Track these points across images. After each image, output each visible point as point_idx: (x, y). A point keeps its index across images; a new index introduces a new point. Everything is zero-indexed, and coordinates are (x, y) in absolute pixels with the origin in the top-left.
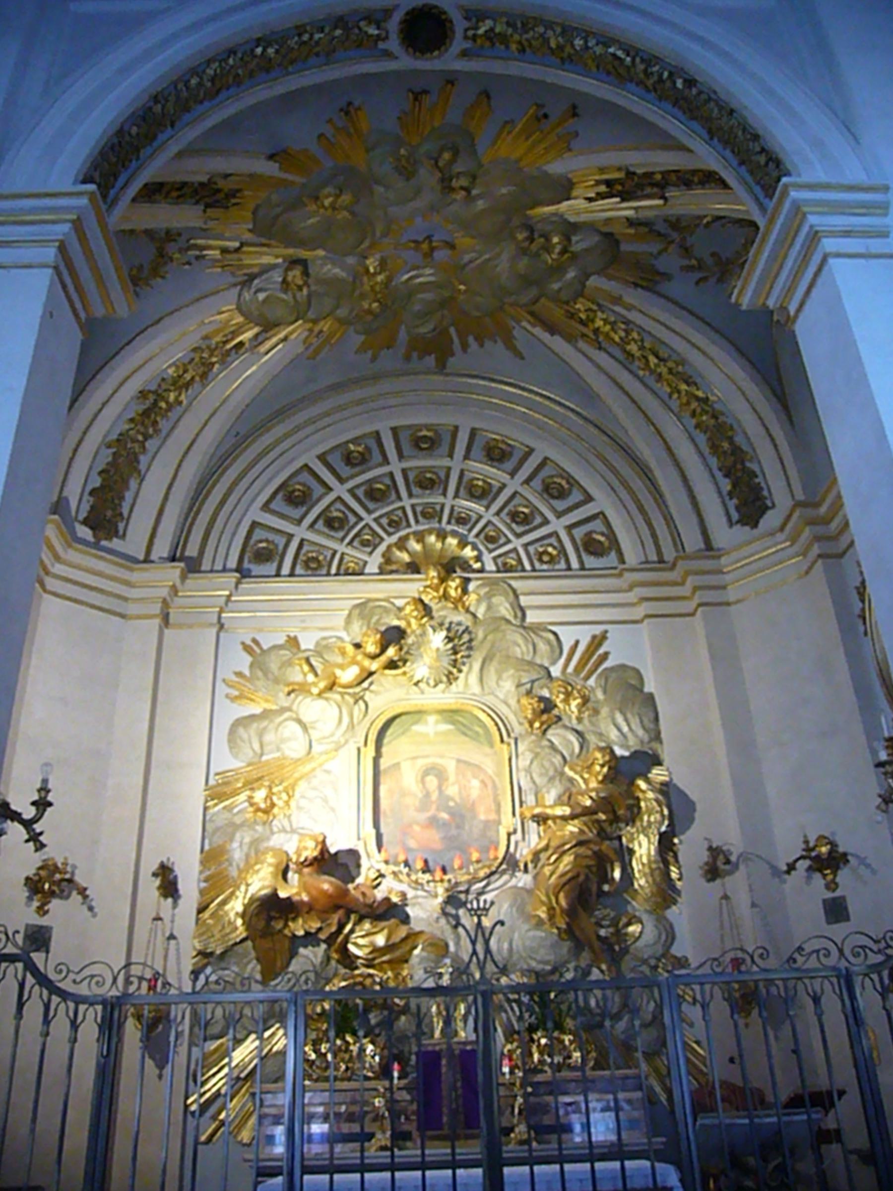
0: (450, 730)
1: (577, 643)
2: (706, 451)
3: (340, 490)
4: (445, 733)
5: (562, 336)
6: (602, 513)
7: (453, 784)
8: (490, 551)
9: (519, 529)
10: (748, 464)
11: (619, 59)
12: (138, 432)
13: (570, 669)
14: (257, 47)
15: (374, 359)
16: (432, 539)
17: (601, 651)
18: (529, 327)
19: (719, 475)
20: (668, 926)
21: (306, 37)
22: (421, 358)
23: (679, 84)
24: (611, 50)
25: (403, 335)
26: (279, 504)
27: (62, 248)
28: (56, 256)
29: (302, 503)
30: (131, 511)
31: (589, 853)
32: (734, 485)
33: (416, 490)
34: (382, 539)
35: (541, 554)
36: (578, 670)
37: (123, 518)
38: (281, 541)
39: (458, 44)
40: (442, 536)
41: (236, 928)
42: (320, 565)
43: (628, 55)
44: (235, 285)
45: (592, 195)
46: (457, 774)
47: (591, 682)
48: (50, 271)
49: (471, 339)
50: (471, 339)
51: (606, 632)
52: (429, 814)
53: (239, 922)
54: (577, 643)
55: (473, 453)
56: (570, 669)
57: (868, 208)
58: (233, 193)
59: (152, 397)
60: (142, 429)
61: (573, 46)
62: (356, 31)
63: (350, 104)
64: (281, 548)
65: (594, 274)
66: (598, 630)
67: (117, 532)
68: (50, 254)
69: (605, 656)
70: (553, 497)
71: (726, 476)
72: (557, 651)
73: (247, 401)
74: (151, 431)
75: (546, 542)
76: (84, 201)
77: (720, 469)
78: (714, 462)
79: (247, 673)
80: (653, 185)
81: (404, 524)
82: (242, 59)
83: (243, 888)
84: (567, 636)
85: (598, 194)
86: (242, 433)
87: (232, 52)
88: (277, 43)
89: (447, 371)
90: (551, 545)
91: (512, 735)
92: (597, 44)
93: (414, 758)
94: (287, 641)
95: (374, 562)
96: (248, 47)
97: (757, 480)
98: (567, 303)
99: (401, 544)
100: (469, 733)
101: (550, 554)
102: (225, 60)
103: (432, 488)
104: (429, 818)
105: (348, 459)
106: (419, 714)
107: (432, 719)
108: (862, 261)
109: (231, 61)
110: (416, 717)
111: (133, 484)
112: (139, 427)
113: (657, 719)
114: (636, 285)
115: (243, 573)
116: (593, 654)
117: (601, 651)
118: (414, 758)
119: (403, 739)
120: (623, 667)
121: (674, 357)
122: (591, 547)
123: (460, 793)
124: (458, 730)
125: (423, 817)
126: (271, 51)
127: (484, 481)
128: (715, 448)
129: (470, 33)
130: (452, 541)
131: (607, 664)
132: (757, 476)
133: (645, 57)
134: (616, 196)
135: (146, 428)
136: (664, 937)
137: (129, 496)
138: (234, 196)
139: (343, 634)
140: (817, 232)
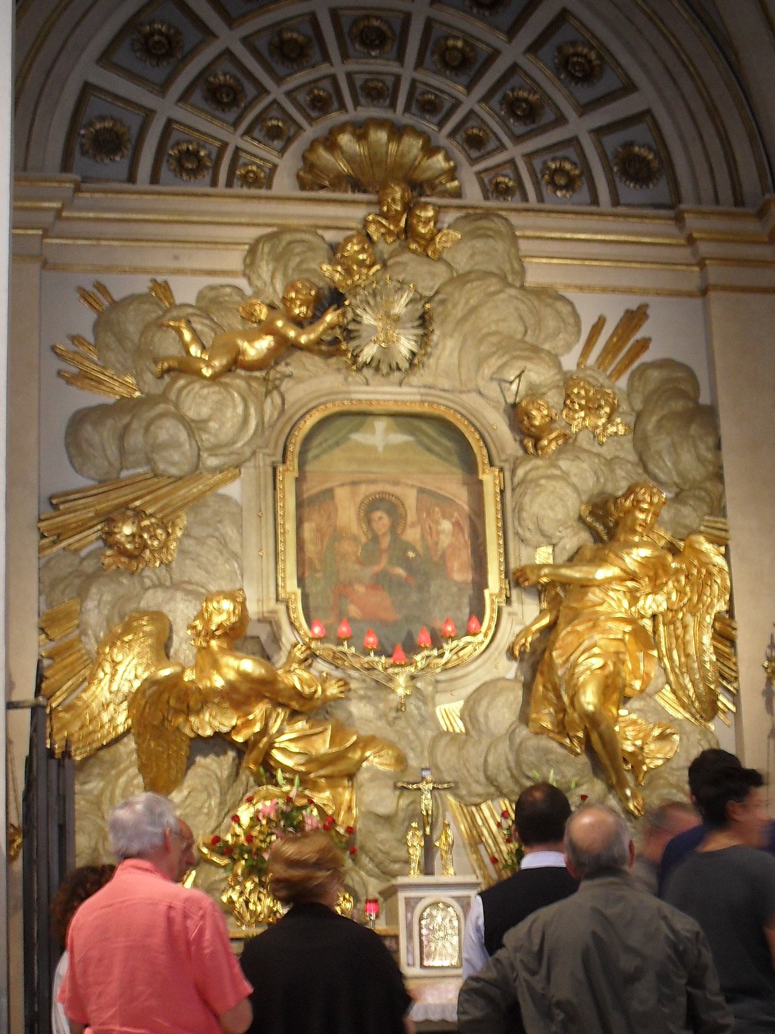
0: (406, 443)
4: (400, 448)
7: (413, 525)
9: (519, 129)
36: (602, 361)
38: (133, 121)
46: (419, 511)
52: (376, 568)
64: (134, 131)
69: (644, 345)
75: (560, 154)
83: (108, 668)
90: (566, 159)
93: (354, 483)
104: (377, 575)
107: (380, 425)
110: (357, 420)
113: (718, 446)
117: (638, 335)
118: (354, 483)
119: (337, 453)
123: (423, 537)
124: (420, 443)
131: (646, 357)
139: (242, 283)
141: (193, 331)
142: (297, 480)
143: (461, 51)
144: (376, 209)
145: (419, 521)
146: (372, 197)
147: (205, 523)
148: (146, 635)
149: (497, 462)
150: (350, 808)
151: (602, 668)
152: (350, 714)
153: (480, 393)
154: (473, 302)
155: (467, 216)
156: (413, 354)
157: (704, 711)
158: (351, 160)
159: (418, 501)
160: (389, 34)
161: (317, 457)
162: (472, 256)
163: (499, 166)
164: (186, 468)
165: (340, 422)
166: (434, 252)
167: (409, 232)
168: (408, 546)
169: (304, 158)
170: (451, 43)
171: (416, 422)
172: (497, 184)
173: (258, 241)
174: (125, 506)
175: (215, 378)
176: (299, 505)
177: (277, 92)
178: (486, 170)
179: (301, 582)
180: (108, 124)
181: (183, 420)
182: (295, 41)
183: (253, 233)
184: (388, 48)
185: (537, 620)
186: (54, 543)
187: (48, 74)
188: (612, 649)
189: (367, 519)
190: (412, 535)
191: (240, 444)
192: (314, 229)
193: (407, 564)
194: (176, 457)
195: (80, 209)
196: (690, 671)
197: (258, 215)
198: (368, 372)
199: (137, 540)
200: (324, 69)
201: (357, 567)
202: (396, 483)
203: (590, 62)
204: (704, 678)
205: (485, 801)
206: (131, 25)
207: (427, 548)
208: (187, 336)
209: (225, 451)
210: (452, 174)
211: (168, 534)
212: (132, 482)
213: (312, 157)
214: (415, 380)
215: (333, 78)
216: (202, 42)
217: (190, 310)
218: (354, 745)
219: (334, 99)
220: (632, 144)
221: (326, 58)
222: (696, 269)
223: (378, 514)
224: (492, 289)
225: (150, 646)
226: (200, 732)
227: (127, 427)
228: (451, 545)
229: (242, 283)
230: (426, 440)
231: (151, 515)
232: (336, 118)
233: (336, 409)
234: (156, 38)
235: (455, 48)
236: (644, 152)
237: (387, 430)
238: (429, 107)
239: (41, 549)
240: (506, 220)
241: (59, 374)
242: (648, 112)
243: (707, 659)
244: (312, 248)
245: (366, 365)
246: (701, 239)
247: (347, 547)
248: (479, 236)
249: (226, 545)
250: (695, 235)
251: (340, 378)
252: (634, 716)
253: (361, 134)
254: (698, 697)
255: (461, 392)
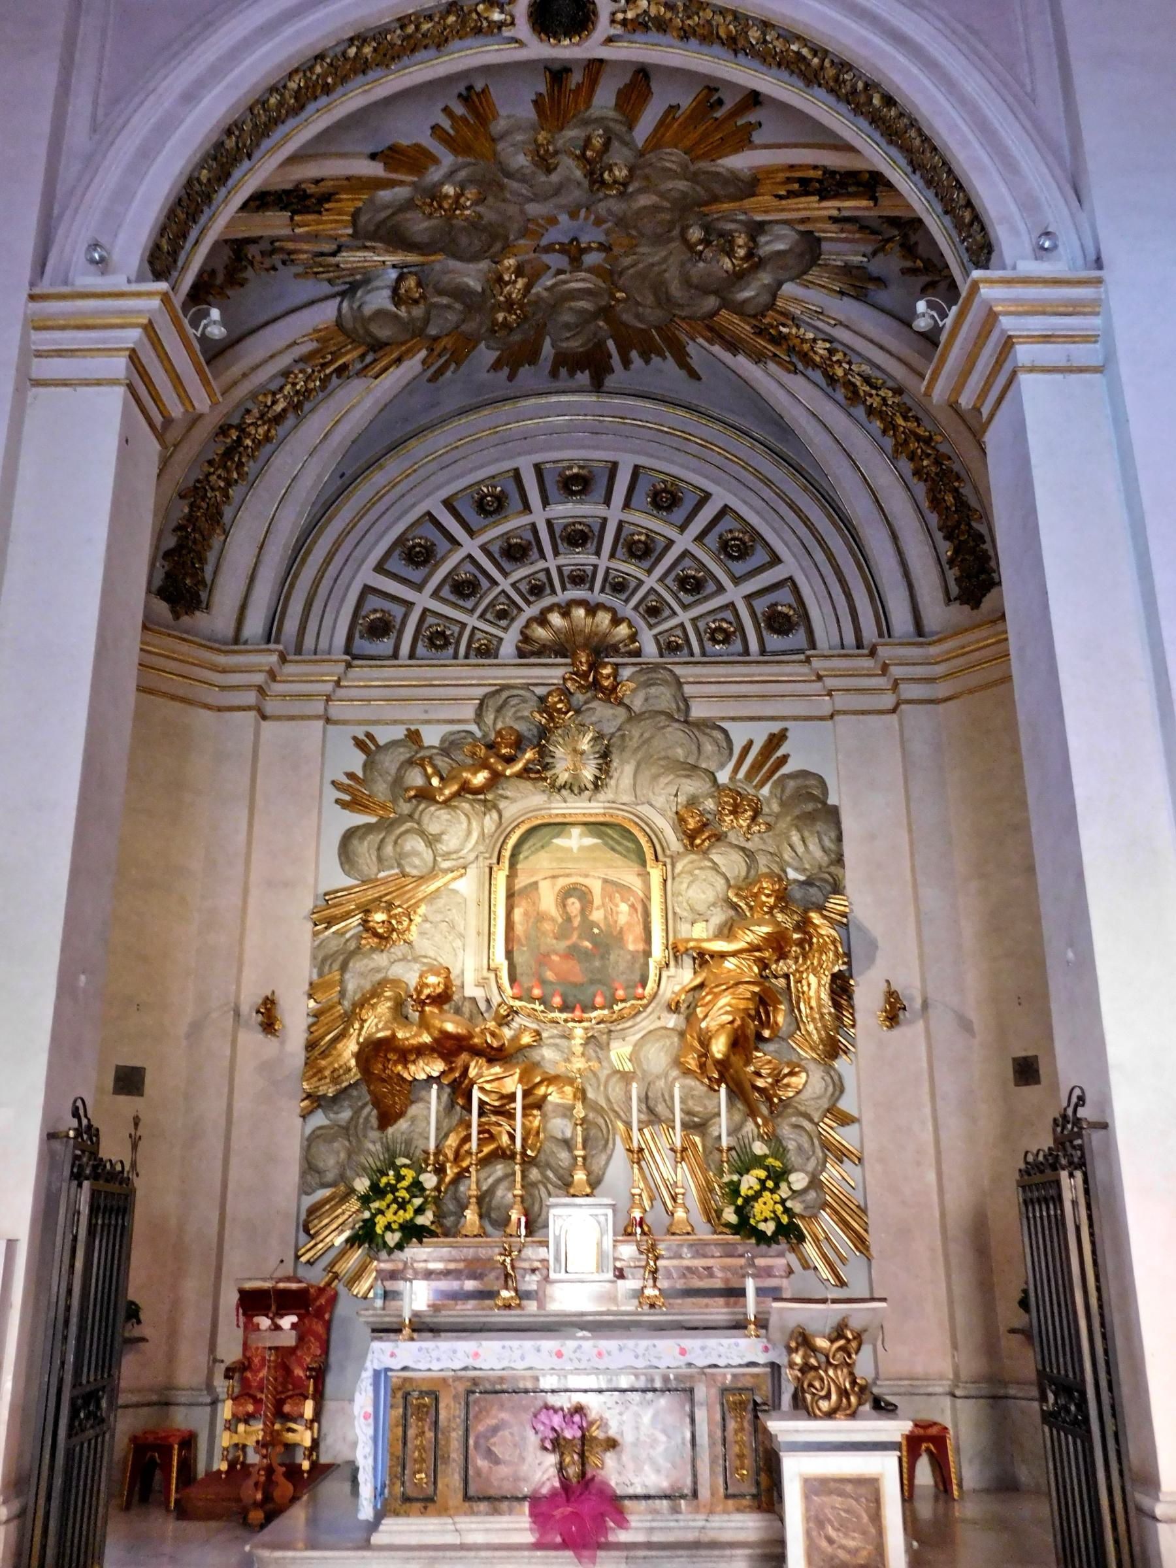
0: (595, 845)
1: (750, 743)
2: (925, 505)
3: (471, 546)
4: (591, 848)
5: (748, 356)
6: (791, 578)
7: (598, 909)
8: (651, 627)
9: (687, 599)
10: (974, 524)
11: (804, 58)
12: (219, 477)
13: (741, 775)
14: (350, 47)
15: (511, 378)
16: (580, 612)
17: (779, 753)
18: (706, 344)
19: (939, 536)
20: (836, 1078)
21: (411, 29)
22: (572, 374)
23: (876, 101)
24: (794, 47)
25: (547, 349)
26: (396, 564)
27: (134, 357)
28: (127, 368)
29: (425, 562)
30: (215, 573)
31: (749, 995)
32: (956, 551)
33: (562, 547)
34: (520, 609)
35: (714, 631)
36: (749, 776)
37: (205, 586)
38: (397, 611)
39: (603, 27)
40: (592, 610)
41: (350, 1070)
42: (447, 643)
43: (815, 55)
44: (333, 296)
45: (783, 193)
46: (603, 897)
47: (765, 791)
48: (120, 391)
49: (634, 354)
50: (634, 354)
51: (786, 729)
52: (568, 943)
53: (353, 1062)
54: (750, 743)
55: (634, 502)
56: (741, 775)
57: (1074, 309)
58: (328, 197)
59: (234, 434)
60: (224, 474)
61: (747, 38)
62: (474, 16)
63: (470, 88)
64: (399, 620)
65: (787, 281)
66: (775, 727)
67: (200, 602)
68: (119, 366)
69: (784, 759)
70: (730, 556)
71: (947, 538)
72: (727, 752)
73: (354, 436)
74: (235, 476)
75: (719, 616)
76: (155, 303)
77: (940, 529)
78: (933, 519)
79: (360, 774)
80: (858, 184)
81: (548, 591)
82: (331, 65)
83: (357, 1026)
84: (740, 734)
85: (788, 192)
86: (349, 473)
87: (320, 57)
88: (374, 39)
89: (605, 389)
90: (723, 620)
91: (668, 852)
92: (778, 38)
93: (554, 877)
94: (406, 736)
95: (510, 640)
96: (339, 49)
97: (984, 547)
98: (755, 316)
99: (542, 620)
100: (618, 848)
101: (724, 631)
102: (311, 69)
103: (583, 545)
104: (569, 947)
105: (481, 507)
106: (561, 826)
107: (576, 831)
108: (1058, 377)
109: (318, 69)
110: (558, 829)
111: (217, 541)
112: (220, 471)
113: (839, 839)
114: (842, 293)
115: (352, 655)
116: (768, 757)
117: (779, 753)
118: (554, 877)
119: (543, 854)
120: (804, 774)
121: (890, 384)
122: (778, 623)
123: (606, 918)
124: (606, 844)
125: (562, 945)
126: (367, 50)
127: (647, 535)
128: (936, 503)
129: (620, 16)
130: (604, 619)
131: (785, 770)
132: (984, 542)
133: (836, 60)
134: (813, 194)
135: (228, 471)
136: (831, 1089)
137: (211, 557)
138: (328, 200)
139: (473, 728)
140: (1010, 337)
141: (434, 766)
142: (508, 877)
143: (645, 543)
144: (571, 669)
145: (603, 905)
146: (568, 661)
147: (439, 911)
148: (388, 999)
149: (661, 857)
150: (538, 1133)
151: (732, 1022)
152: (543, 1057)
153: (651, 805)
154: (647, 735)
155: (642, 669)
156: (597, 778)
157: (828, 1052)
158: (557, 632)
159: (603, 889)
160: (590, 534)
161: (527, 858)
162: (646, 700)
163: (671, 629)
164: (425, 871)
165: (545, 830)
166: (616, 699)
167: (596, 685)
168: (594, 924)
169: (522, 633)
170: (636, 537)
171: (603, 828)
172: (670, 642)
173: (485, 696)
174: (379, 899)
175: (446, 803)
176: (510, 895)
177: (505, 584)
178: (660, 633)
179: (509, 954)
180: (378, 615)
181: (422, 833)
182: (519, 545)
183: (481, 692)
184: (589, 545)
185: (692, 980)
186: (326, 928)
187: (336, 580)
188: (742, 1007)
189: (562, 904)
190: (597, 916)
191: (465, 851)
192: (526, 687)
193: (593, 938)
194: (417, 861)
195: (353, 680)
196: (813, 1020)
197: (483, 678)
198: (563, 792)
199: (386, 925)
200: (541, 565)
201: (555, 941)
202: (587, 876)
203: (744, 543)
204: (825, 1027)
205: (647, 1126)
206: (400, 541)
207: (608, 925)
208: (430, 770)
209: (454, 856)
210: (633, 638)
211: (411, 920)
212: (385, 882)
213: (528, 632)
214: (601, 796)
215: (547, 571)
216: (450, 551)
217: (435, 751)
218: (541, 1082)
219: (547, 586)
220: (776, 604)
221: (543, 556)
222: (827, 698)
223: (571, 900)
224: (662, 724)
225: (389, 1008)
226: (417, 1077)
227: (382, 840)
228: (629, 924)
229: (473, 728)
230: (611, 842)
231: (399, 906)
232: (547, 601)
233: (539, 822)
234: (418, 549)
235: (639, 541)
236: (785, 610)
237: (581, 835)
238: (619, 587)
239: (316, 934)
240: (671, 671)
241: (337, 801)
242: (791, 578)
243: (825, 1011)
244: (525, 701)
245: (564, 787)
246: (827, 676)
247: (547, 926)
248: (652, 685)
249: (454, 927)
250: (821, 673)
251: (544, 797)
252: (769, 1057)
253: (566, 613)
254: (821, 1040)
255: (637, 804)
